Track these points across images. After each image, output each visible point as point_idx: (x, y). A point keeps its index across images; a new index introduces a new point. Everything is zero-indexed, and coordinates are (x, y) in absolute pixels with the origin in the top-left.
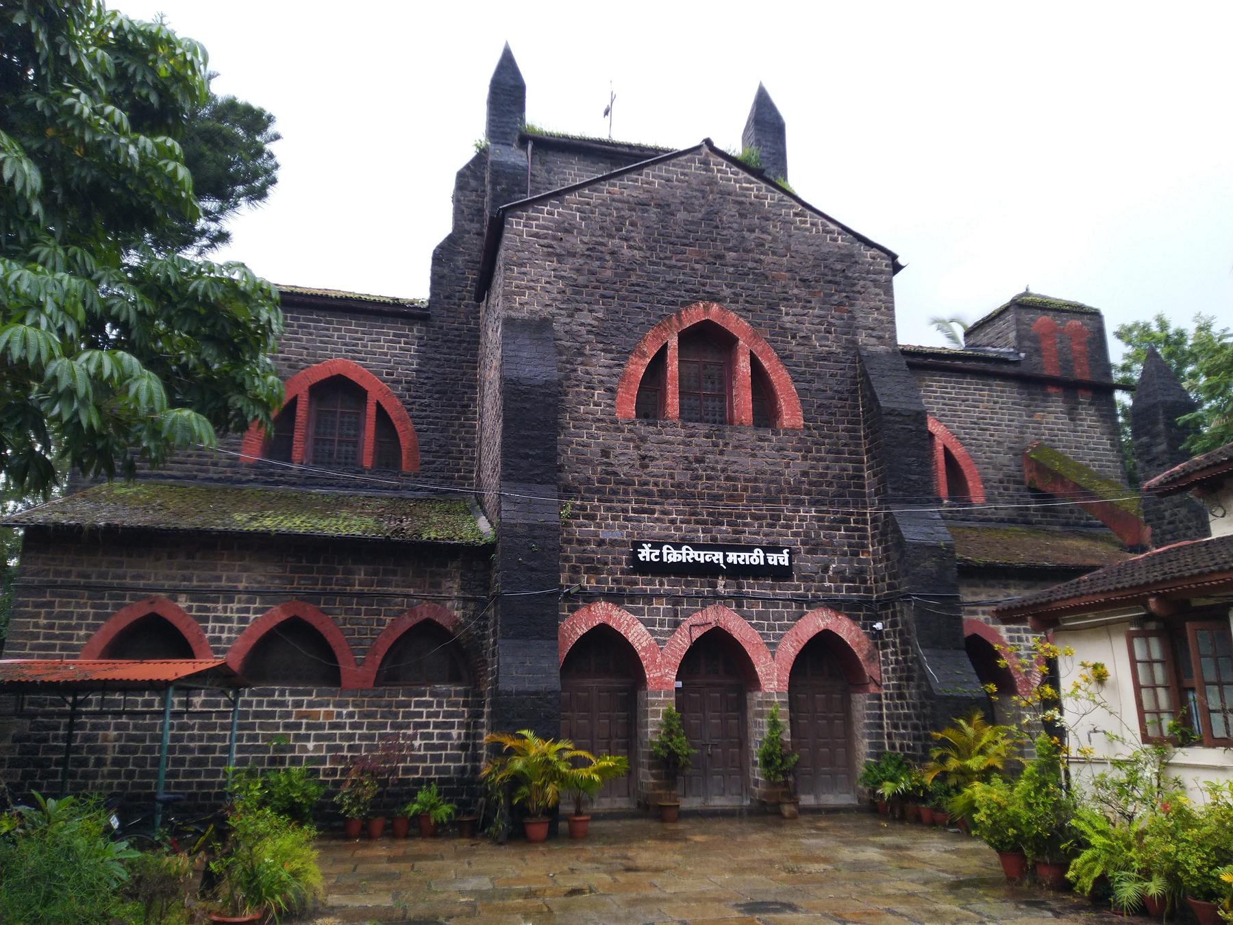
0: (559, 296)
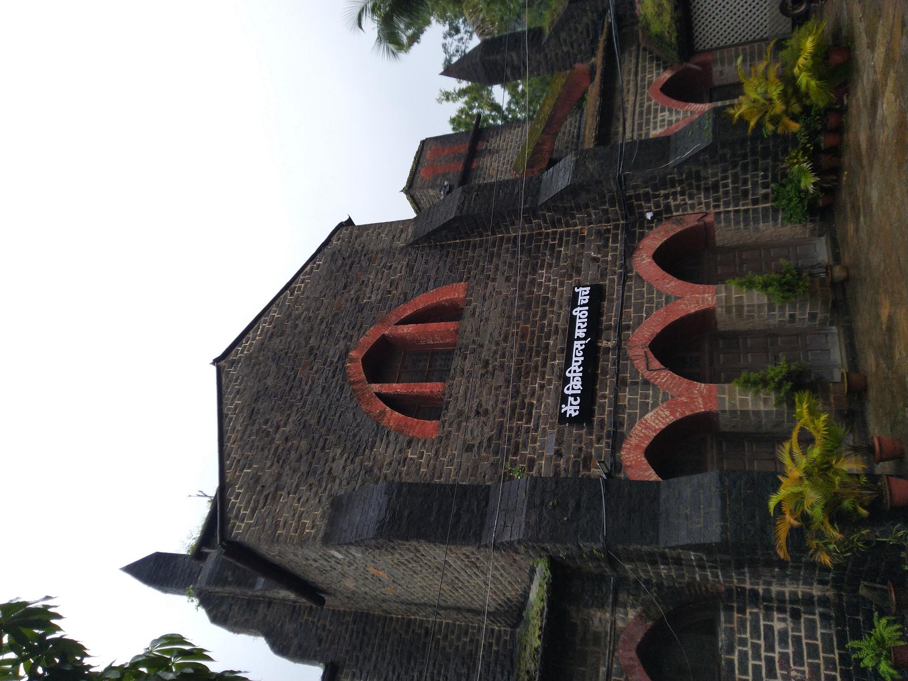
0: (314, 489)
